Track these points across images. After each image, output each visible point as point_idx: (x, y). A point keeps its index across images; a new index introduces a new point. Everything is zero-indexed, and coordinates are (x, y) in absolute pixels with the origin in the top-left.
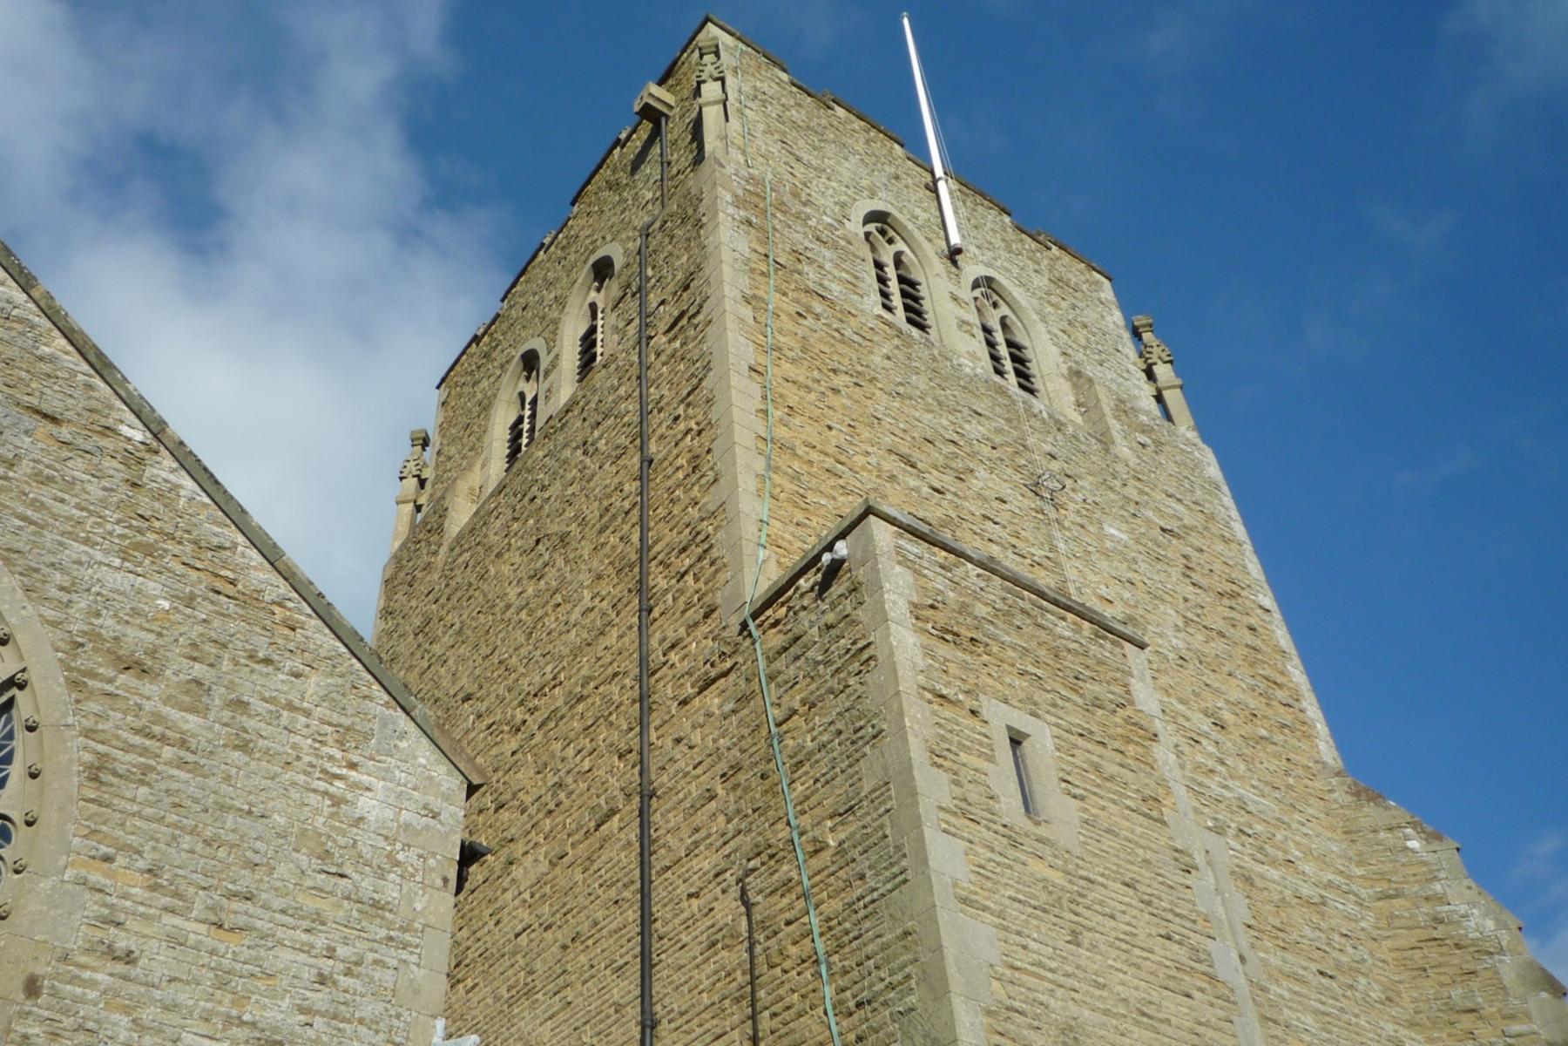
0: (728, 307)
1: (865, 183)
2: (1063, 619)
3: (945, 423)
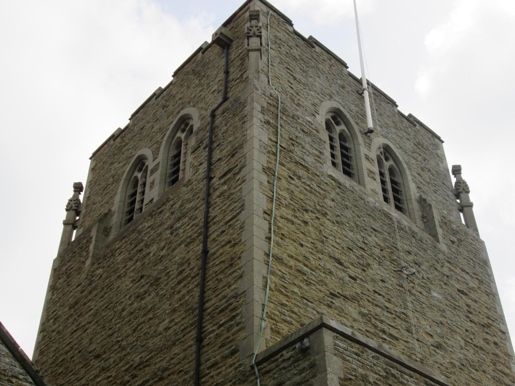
0: (255, 176)
1: (327, 91)
2: (412, 377)
3: (359, 237)
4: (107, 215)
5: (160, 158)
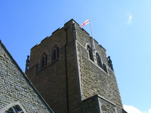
4: (38, 64)
5: (50, 53)
